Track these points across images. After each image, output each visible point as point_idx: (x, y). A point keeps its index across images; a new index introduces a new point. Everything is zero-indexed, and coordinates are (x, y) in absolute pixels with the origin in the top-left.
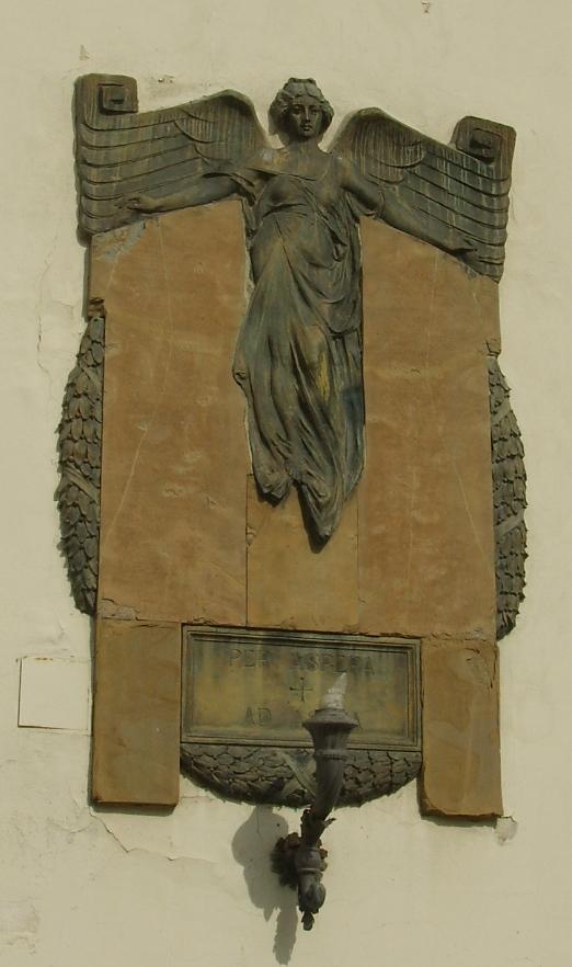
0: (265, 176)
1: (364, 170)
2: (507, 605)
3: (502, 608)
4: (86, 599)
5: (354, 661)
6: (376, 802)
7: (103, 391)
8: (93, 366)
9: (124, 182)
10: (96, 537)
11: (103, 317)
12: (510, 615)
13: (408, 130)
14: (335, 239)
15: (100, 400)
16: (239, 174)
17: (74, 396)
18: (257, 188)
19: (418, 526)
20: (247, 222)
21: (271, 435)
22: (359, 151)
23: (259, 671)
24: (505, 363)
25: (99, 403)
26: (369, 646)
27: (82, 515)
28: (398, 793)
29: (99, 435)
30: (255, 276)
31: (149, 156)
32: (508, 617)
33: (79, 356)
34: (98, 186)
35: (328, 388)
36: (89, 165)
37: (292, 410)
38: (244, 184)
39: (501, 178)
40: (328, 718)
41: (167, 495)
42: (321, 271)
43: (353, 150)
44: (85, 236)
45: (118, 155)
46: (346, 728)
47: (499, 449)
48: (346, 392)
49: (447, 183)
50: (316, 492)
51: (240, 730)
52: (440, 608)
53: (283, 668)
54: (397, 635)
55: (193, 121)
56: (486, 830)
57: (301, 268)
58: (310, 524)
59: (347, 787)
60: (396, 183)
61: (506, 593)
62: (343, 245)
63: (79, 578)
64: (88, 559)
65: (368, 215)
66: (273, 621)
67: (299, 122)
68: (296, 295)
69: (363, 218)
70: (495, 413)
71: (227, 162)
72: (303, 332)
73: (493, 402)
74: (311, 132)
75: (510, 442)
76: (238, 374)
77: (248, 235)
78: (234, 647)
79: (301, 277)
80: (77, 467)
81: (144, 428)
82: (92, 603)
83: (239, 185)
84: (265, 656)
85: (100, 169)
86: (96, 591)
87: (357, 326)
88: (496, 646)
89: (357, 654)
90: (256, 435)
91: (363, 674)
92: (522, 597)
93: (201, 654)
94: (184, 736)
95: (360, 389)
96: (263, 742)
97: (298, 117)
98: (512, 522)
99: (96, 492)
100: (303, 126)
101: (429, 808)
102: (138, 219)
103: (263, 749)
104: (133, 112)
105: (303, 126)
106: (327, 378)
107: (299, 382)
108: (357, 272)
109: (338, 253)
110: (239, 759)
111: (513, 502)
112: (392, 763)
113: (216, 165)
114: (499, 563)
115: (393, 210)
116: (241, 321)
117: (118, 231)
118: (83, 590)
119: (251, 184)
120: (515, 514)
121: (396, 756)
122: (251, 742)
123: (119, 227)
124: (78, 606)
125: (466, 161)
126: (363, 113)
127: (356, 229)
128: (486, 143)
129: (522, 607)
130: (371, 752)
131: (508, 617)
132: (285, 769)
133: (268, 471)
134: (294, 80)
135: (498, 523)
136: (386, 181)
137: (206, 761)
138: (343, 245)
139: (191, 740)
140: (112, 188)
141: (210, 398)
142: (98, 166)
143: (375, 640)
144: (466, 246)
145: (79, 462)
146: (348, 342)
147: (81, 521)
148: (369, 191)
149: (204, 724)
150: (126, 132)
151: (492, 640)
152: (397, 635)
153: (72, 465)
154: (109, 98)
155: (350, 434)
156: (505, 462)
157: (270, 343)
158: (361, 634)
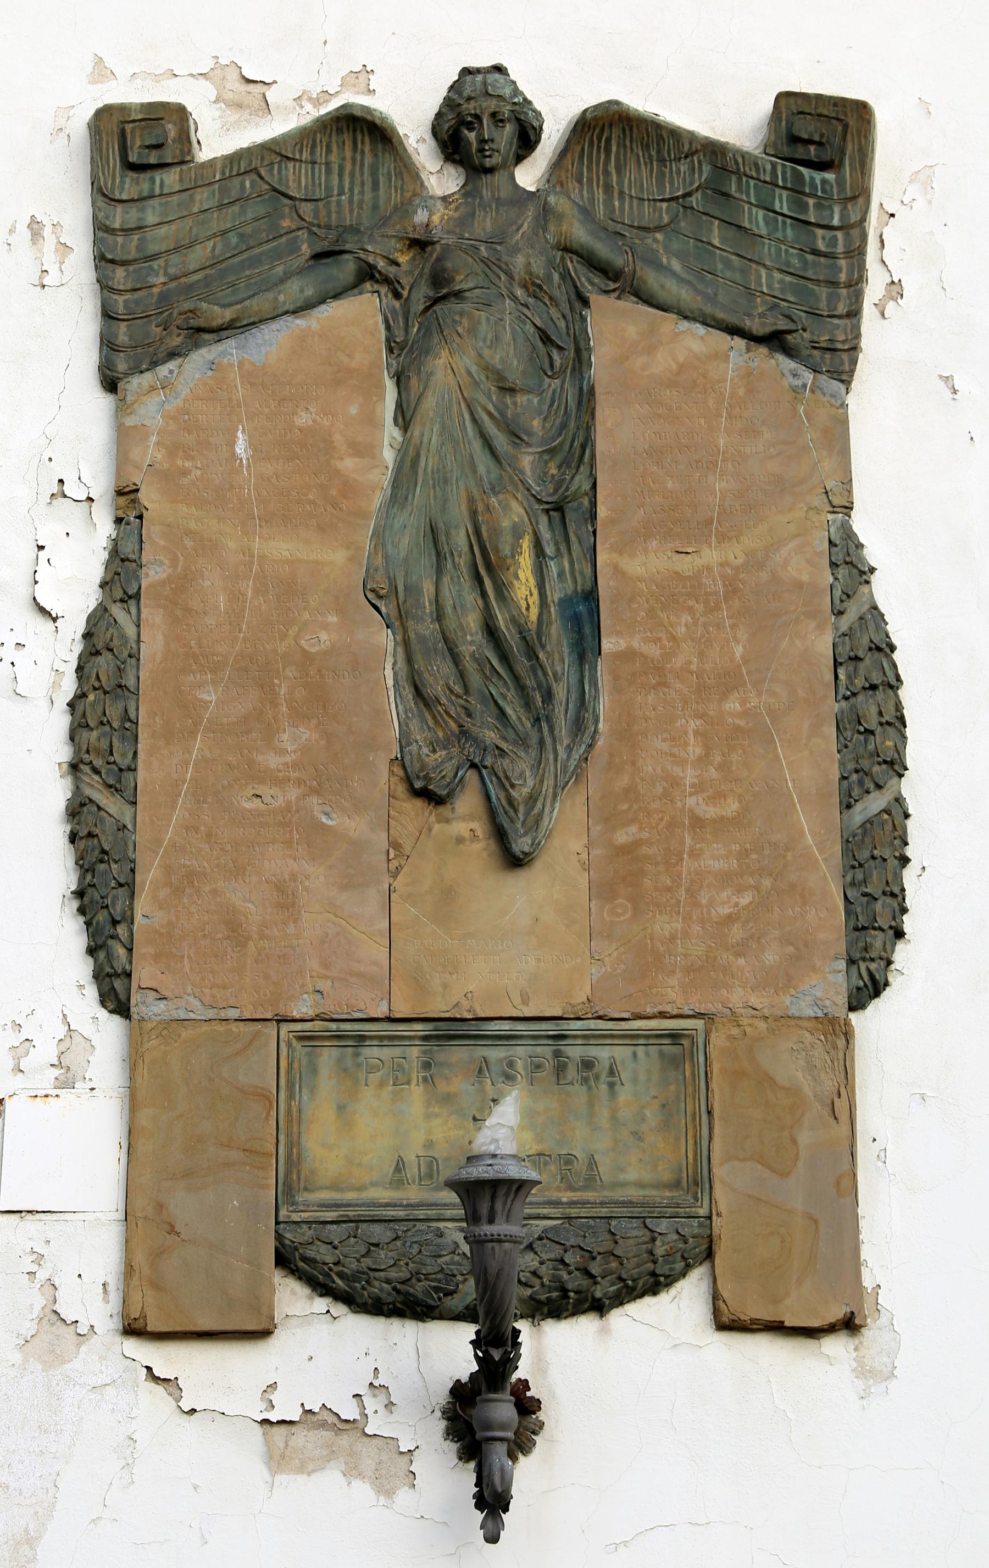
0: (420, 244)
1: (600, 211)
2: (866, 949)
3: (857, 955)
4: (113, 989)
5: (587, 1064)
6: (633, 1308)
7: (138, 641)
8: (122, 601)
9: (173, 285)
10: (129, 886)
11: (140, 517)
12: (873, 966)
13: (675, 134)
14: (546, 338)
15: (134, 656)
16: (369, 248)
17: (91, 654)
18: (404, 267)
19: (697, 822)
20: (388, 328)
21: (435, 688)
22: (590, 180)
23: (416, 1092)
24: (860, 524)
25: (133, 661)
26: (612, 1036)
27: (104, 852)
28: (673, 1291)
29: (132, 715)
30: (404, 417)
31: (215, 235)
32: (868, 969)
33: (103, 585)
34: (128, 296)
35: (535, 599)
36: (112, 261)
37: (472, 643)
38: (381, 264)
39: (849, 194)
40: (479, 1172)
41: (248, 805)
42: (521, 399)
43: (580, 181)
44: (110, 384)
45: (160, 238)
46: (519, 1187)
47: (849, 677)
48: (565, 603)
49: (756, 220)
50: (507, 778)
51: (383, 1194)
52: (741, 961)
53: (461, 1085)
54: (663, 1015)
55: (291, 165)
56: (835, 1346)
57: (483, 399)
58: (500, 835)
59: (570, 1286)
60: (659, 228)
61: (864, 928)
62: (560, 348)
63: (102, 955)
64: (115, 923)
65: (607, 292)
66: (439, 1008)
67: (474, 145)
68: (477, 445)
69: (594, 298)
70: (841, 613)
71: (355, 230)
72: (488, 508)
73: (838, 593)
74: (495, 160)
75: (867, 661)
76: (373, 591)
77: (390, 350)
78: (372, 1053)
79: (486, 418)
80: (96, 771)
81: (210, 696)
82: (122, 997)
83: (372, 267)
84: (427, 1066)
85: (131, 268)
86: (129, 975)
87: (587, 486)
88: (847, 1023)
89: (593, 1052)
90: (408, 693)
91: (604, 1087)
92: (899, 934)
93: (314, 1070)
94: (283, 1213)
95: (591, 596)
96: (421, 1214)
97: (472, 136)
98: (875, 803)
99: (128, 811)
100: (481, 150)
101: (725, 1319)
102: (197, 346)
103: (420, 1226)
104: (184, 158)
105: (481, 150)
106: (532, 582)
107: (484, 594)
108: (587, 399)
109: (552, 366)
110: (377, 1245)
111: (876, 769)
112: (653, 1240)
113: (332, 236)
114: (849, 878)
115: (652, 280)
116: (377, 500)
117: (163, 370)
118: (109, 975)
119: (396, 263)
120: (879, 787)
121: (663, 1226)
122: (401, 1214)
123: (164, 362)
124: (103, 1003)
125: (784, 171)
126: (588, 115)
127: (583, 319)
128: (817, 138)
129: (901, 954)
130: (614, 1223)
131: (868, 969)
132: (457, 1258)
133: (425, 750)
134: (466, 72)
135: (849, 806)
136: (639, 228)
137: (323, 1254)
138: (560, 348)
139: (295, 1217)
140: (152, 295)
141: (324, 636)
142: (124, 263)
143: (623, 1025)
144: (783, 325)
145: (98, 763)
146: (570, 516)
147: (101, 861)
148: (603, 250)
149: (321, 1188)
150: (175, 198)
151: (840, 1010)
152: (663, 1015)
153: (86, 769)
154: (138, 143)
155: (574, 679)
156: (860, 698)
157: (433, 530)
158: (600, 1018)
